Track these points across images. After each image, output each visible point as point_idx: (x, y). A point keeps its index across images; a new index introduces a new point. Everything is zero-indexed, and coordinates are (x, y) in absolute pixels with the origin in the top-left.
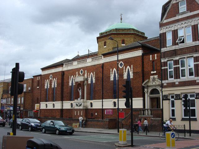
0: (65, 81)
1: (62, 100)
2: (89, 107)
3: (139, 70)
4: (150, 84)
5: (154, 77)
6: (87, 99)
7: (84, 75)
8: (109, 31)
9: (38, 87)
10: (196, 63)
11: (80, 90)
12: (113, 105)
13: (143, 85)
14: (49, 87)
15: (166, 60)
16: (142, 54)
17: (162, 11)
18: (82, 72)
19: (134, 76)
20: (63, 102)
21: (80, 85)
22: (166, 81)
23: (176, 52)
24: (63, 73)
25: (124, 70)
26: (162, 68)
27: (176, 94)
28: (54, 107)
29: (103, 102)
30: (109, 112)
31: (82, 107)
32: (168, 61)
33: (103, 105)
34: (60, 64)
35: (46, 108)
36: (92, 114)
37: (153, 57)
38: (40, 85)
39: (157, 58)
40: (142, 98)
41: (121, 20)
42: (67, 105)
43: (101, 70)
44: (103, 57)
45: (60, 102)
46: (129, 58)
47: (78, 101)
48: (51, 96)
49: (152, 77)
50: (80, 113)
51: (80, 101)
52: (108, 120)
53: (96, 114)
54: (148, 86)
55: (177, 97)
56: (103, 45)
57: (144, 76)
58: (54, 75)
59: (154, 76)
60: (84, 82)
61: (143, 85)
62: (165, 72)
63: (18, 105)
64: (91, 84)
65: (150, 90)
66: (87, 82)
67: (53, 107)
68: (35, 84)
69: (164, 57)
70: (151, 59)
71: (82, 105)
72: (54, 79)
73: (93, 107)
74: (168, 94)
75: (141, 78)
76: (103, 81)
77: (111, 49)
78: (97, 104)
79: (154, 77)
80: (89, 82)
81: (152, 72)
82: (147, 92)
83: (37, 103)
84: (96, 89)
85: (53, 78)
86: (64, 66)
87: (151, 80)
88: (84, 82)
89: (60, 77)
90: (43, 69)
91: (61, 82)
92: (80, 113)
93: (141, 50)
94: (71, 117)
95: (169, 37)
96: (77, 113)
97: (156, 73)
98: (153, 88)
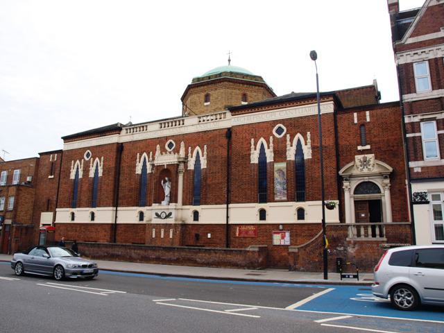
0: (124, 165)
1: (116, 204)
2: (190, 221)
3: (329, 141)
4: (355, 172)
7: (177, 151)
8: (216, 76)
10: (417, 134)
11: (167, 184)
12: (90, 218)
13: (340, 173)
14: (80, 176)
15: (416, 119)
17: (391, 24)
18: (170, 145)
19: (313, 155)
20: (119, 208)
21: (167, 173)
22: (421, 163)
24: (120, 147)
25: (91, 164)
26: (408, 135)
29: (118, 212)
30: (247, 232)
31: (173, 219)
32: (422, 120)
33: (228, 217)
34: (115, 129)
36: (197, 236)
38: (57, 172)
40: (52, 213)
42: (128, 215)
43: (225, 141)
44: (229, 114)
45: (111, 208)
46: (301, 117)
47: (162, 207)
48: (91, 195)
49: (358, 158)
50: (167, 233)
52: (257, 250)
53: (209, 236)
54: (351, 176)
56: (203, 99)
57: (342, 155)
58: (97, 151)
59: (366, 155)
60: (178, 165)
62: (414, 144)
63: (24, 218)
64: (194, 172)
65: (354, 184)
66: (186, 167)
70: (356, 121)
71: (173, 216)
73: (97, 221)
75: (334, 158)
77: (220, 109)
78: (212, 215)
80: (191, 166)
81: (360, 148)
82: (349, 187)
84: (208, 182)
86: (124, 132)
88: (178, 165)
89: (113, 154)
90: (67, 139)
91: (114, 165)
92: (167, 233)
94: (142, 242)
96: (158, 233)
97: (370, 150)
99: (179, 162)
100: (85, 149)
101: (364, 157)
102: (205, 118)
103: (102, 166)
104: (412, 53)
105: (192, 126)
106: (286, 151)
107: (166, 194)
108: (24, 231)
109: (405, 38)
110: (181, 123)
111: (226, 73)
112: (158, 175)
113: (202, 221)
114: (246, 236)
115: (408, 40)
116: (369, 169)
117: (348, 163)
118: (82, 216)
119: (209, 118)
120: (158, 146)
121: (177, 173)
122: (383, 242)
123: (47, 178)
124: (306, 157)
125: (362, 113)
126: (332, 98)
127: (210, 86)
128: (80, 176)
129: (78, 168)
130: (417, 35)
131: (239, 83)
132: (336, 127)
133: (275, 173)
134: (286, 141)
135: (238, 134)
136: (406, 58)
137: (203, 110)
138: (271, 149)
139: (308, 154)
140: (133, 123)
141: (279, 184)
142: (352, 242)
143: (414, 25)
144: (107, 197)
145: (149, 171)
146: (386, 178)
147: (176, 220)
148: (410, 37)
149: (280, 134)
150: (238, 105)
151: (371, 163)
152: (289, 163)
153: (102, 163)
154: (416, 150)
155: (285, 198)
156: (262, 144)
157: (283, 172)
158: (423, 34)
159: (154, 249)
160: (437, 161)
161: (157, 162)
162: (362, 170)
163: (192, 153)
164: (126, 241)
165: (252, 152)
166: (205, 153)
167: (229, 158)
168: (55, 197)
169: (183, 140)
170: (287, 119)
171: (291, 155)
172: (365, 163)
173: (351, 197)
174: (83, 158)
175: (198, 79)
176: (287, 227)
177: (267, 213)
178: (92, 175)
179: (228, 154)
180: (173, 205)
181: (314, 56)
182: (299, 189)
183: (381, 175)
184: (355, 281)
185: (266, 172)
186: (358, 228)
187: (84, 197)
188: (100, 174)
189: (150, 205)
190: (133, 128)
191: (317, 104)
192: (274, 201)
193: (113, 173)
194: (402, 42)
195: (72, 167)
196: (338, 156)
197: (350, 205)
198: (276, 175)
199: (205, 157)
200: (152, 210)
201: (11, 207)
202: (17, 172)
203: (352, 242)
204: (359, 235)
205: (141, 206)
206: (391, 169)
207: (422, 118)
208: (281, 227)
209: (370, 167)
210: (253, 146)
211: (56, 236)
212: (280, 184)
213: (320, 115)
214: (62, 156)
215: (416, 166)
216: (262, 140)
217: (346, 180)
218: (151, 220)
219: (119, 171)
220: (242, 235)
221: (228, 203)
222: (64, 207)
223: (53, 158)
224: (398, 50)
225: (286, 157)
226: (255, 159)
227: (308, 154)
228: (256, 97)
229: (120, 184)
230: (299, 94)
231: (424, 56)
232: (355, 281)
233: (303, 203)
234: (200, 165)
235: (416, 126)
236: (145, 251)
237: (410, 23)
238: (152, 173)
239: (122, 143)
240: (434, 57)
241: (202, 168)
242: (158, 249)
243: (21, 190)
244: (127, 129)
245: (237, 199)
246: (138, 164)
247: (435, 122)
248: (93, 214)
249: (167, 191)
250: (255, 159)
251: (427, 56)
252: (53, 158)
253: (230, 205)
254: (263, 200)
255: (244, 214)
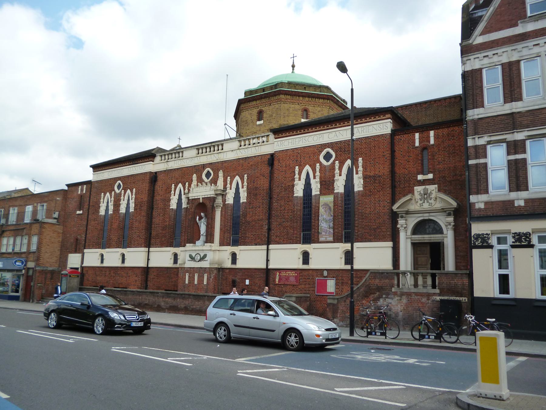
0: (157, 198)
2: (228, 264)
3: (384, 170)
4: (413, 207)
5: (426, 190)
6: (222, 244)
7: (214, 182)
8: (271, 87)
9: (78, 212)
10: (482, 161)
13: (395, 208)
14: (111, 212)
15: (481, 141)
16: (392, 130)
17: (463, 18)
18: (208, 175)
19: (365, 186)
20: (151, 249)
21: (204, 207)
22: (524, 195)
23: (513, 119)
24: (154, 177)
25: (122, 198)
26: (471, 162)
27: (518, 231)
28: (102, 262)
29: (151, 254)
30: (287, 278)
31: (208, 262)
32: (489, 143)
33: (268, 260)
34: (148, 156)
35: (301, 266)
37: (425, 139)
38: (86, 206)
39: (435, 141)
40: (390, 244)
41: (293, 69)
42: (161, 257)
43: (266, 170)
44: (272, 136)
47: (197, 248)
48: (119, 233)
49: (418, 189)
51: (200, 246)
53: (247, 282)
54: (408, 213)
55: (520, 241)
56: (255, 117)
57: (397, 185)
58: (128, 182)
59: (427, 187)
61: (395, 208)
62: (477, 174)
63: (50, 262)
65: (412, 221)
66: (224, 201)
67: (100, 261)
68: (72, 203)
69: (477, 133)
70: (417, 144)
72: (129, 191)
73: (127, 264)
74: (489, 232)
75: (389, 190)
76: (271, 198)
78: (251, 257)
79: (426, 190)
80: (230, 200)
81: (420, 177)
83: (76, 252)
85: (125, 190)
86: (158, 159)
87: (417, 196)
89: (146, 186)
90: (96, 168)
93: (390, 120)
95: (492, 84)
96: (192, 279)
98: (416, 222)
99: (216, 194)
100: (116, 179)
101: (425, 189)
102: (255, 141)
103: (133, 200)
104: (481, 55)
105: (232, 152)
106: (334, 181)
107: (202, 233)
108: (49, 276)
109: (474, 37)
110: (220, 147)
111: (281, 84)
112: (193, 210)
113: (240, 265)
114: (287, 283)
115: (478, 39)
116: (430, 204)
117: (404, 196)
118: (112, 258)
119: (261, 140)
120: (195, 175)
121: (213, 209)
122: (434, 294)
123: (75, 211)
124: (356, 189)
125: (425, 134)
126: (389, 116)
127: (263, 100)
128: (111, 212)
129: (129, 200)
130: (489, 32)
131: (299, 96)
132: (393, 152)
133: (321, 208)
134: (334, 169)
135: (281, 161)
136: (474, 63)
137: (255, 131)
138: (318, 179)
139: (358, 185)
140: (182, 147)
141: (325, 222)
142: (399, 293)
143: (486, 18)
144: (139, 236)
145: (184, 205)
146: (449, 215)
147: (210, 264)
148: (480, 35)
149: (328, 161)
150: (297, 122)
151: (433, 196)
152: (336, 196)
153: (134, 196)
154: (481, 183)
155: (331, 239)
156: (308, 174)
157: (330, 208)
158: (496, 31)
159: (183, 296)
160: (505, 195)
161: (192, 195)
162: (421, 205)
163: (231, 184)
164: (158, 288)
165: (295, 183)
166: (245, 183)
167: (270, 189)
168: (83, 236)
169: (222, 168)
170: (336, 143)
171: (339, 186)
172: (426, 196)
173: (407, 238)
174: (114, 190)
175: (250, 92)
176: (332, 273)
177: (310, 256)
178: (123, 210)
179: (270, 185)
180: (208, 246)
181: (342, 67)
182: (349, 229)
183: (443, 210)
184: (382, 339)
185: (311, 207)
186: (415, 275)
187: (114, 238)
188: (132, 210)
189: (184, 246)
190: (168, 154)
191: (350, 127)
192: (318, 242)
193: (145, 208)
194: (470, 42)
195: (102, 200)
196: (393, 187)
197: (406, 249)
198: (322, 210)
199: (245, 188)
200: (186, 251)
201: (34, 248)
202: (29, 209)
203: (399, 293)
204: (416, 285)
205: (176, 246)
206: (454, 204)
207: (489, 139)
208: (325, 273)
209: (432, 201)
210: (297, 176)
211: (86, 278)
212: (326, 222)
213: (353, 140)
214: (91, 188)
215: (478, 201)
216: (308, 168)
217: (402, 217)
218: (184, 263)
219: (153, 205)
220: (282, 283)
221: (268, 244)
222: (93, 247)
223: (82, 190)
224: (466, 50)
225: (333, 189)
226: (299, 191)
227: (358, 185)
228: (320, 111)
229: (154, 220)
230: (361, 108)
231: (496, 59)
232: (382, 339)
233: (124, 250)
234: (311, 190)
235: (481, 151)
236: (174, 299)
237: (481, 17)
238: (187, 208)
239: (156, 173)
240: (471, 69)
241: (241, 201)
242: (187, 296)
243: (44, 228)
244: (161, 156)
245: (278, 239)
246: (337, 177)
247: (505, 145)
248: (176, 256)
249: (203, 229)
250: (299, 191)
251: (500, 58)
252: (82, 190)
253: (271, 246)
254: (307, 240)
255: (285, 257)
